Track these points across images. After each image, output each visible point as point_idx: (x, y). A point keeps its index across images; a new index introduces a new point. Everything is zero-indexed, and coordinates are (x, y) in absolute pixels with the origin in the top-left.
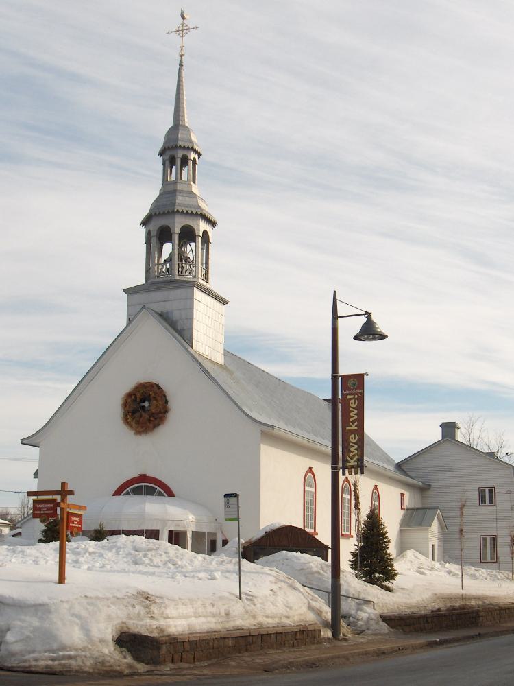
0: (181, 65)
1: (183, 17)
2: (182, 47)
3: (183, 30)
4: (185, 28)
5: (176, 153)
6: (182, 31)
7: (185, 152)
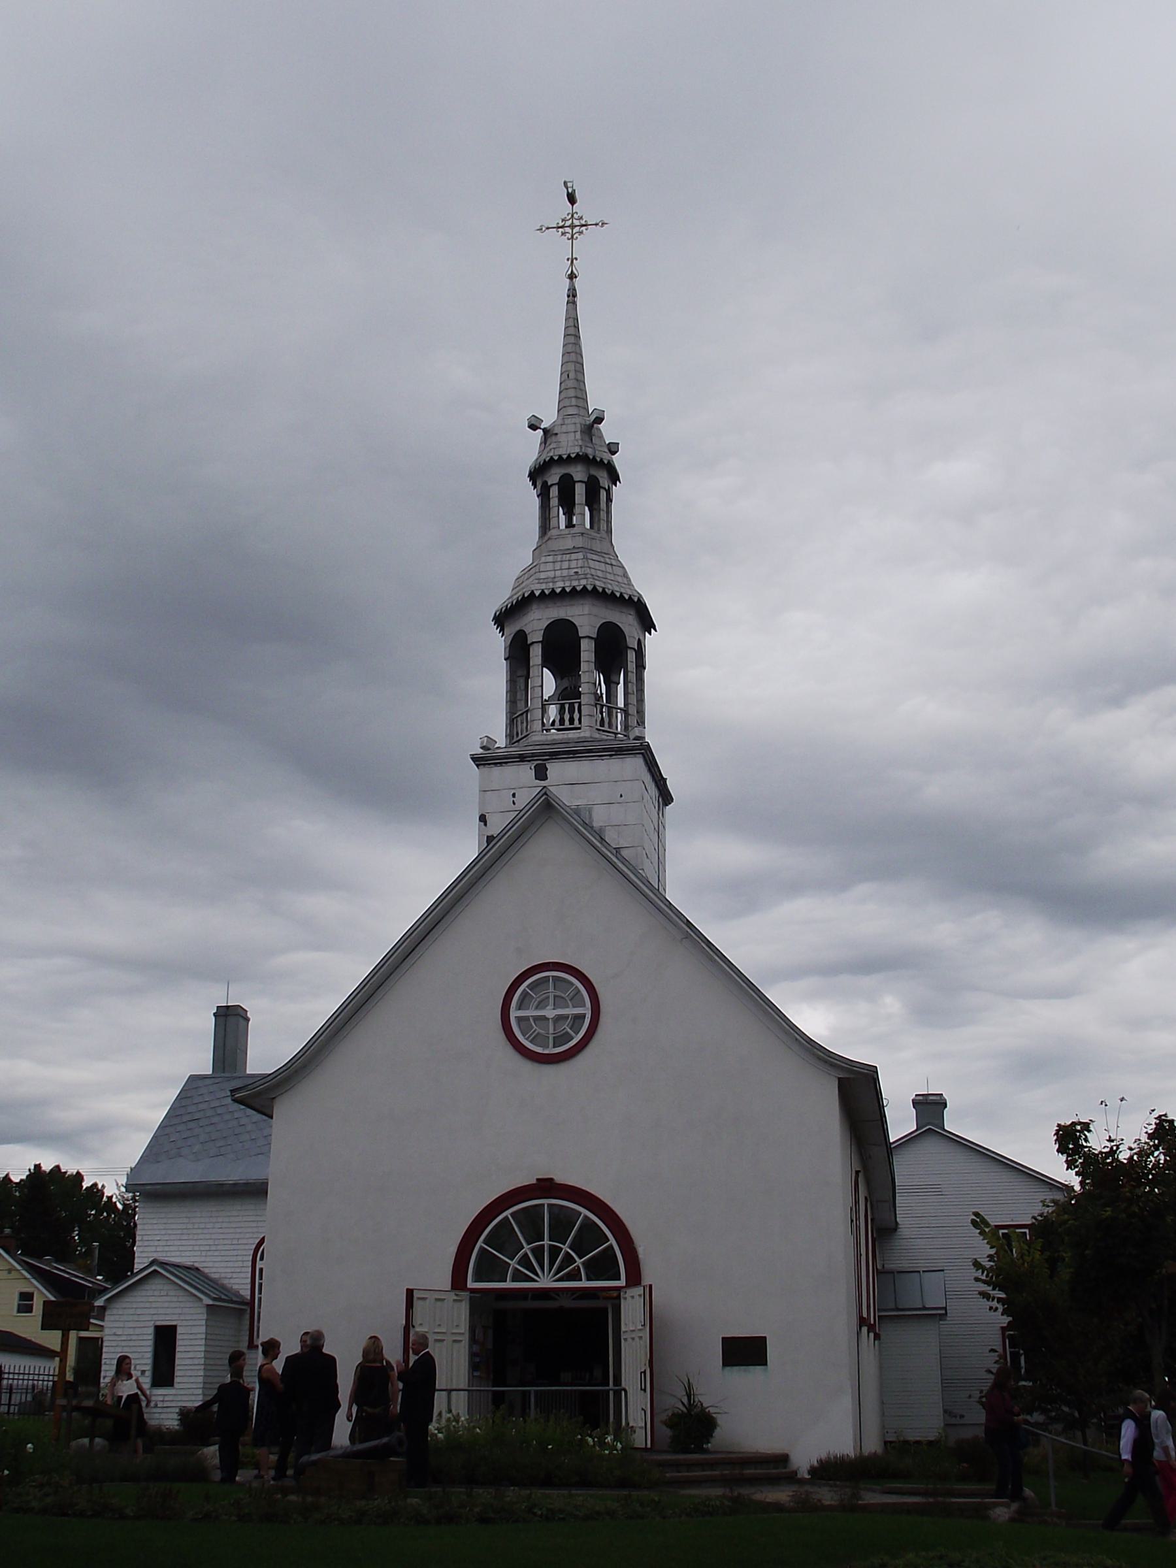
0: (572, 294)
1: (572, 199)
2: (572, 276)
3: (572, 226)
4: (576, 222)
5: (576, 476)
6: (572, 227)
7: (594, 472)
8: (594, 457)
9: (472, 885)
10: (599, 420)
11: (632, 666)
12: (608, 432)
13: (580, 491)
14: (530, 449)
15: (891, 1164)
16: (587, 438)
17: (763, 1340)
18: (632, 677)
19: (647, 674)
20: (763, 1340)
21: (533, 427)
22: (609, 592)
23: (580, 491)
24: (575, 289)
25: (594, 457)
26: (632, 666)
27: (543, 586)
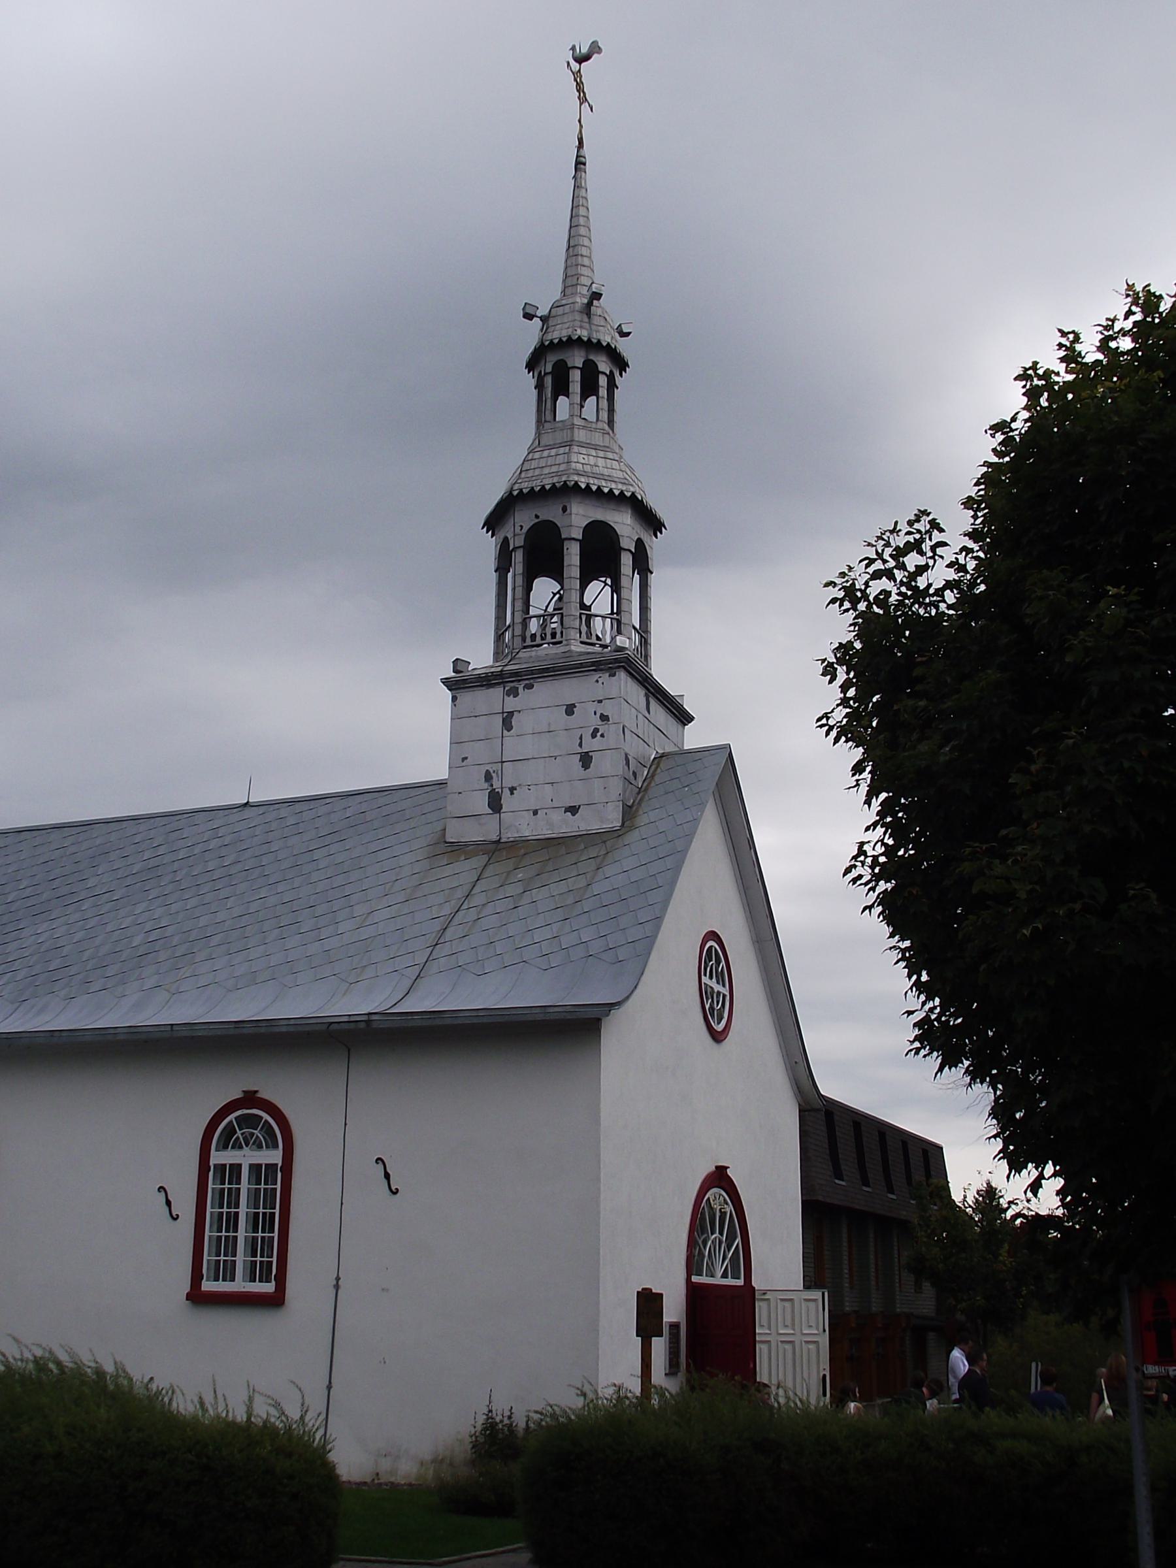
8: (589, 340)
9: (554, 669)
10: (597, 296)
11: (603, 392)
12: (612, 309)
13: (576, 376)
14: (530, 335)
15: (690, 752)
16: (586, 320)
17: (661, 1295)
18: (604, 404)
19: (643, 978)
20: (661, 1295)
21: (528, 316)
22: (595, 341)
23: (576, 376)
24: (538, 428)
25: (589, 340)
26: (603, 392)
27: (555, 480)
